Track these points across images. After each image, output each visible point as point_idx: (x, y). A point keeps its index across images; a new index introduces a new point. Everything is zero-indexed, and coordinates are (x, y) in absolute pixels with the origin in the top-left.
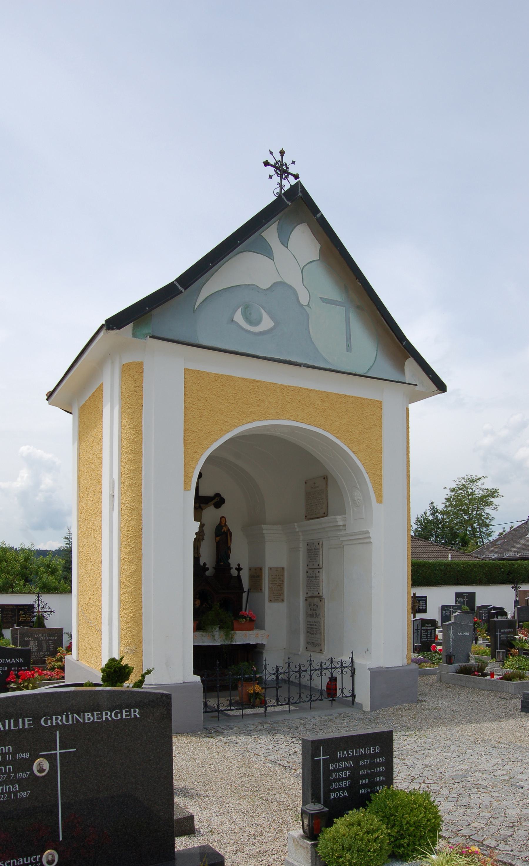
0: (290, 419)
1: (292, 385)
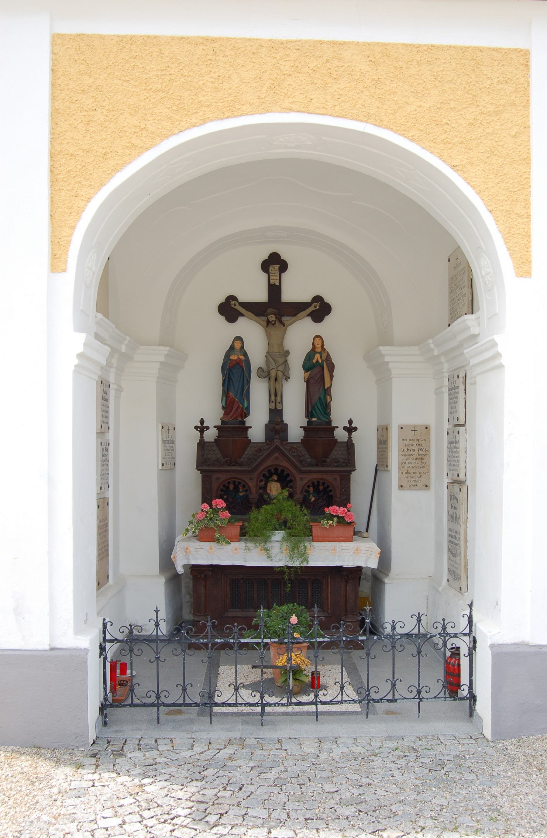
0: (291, 110)
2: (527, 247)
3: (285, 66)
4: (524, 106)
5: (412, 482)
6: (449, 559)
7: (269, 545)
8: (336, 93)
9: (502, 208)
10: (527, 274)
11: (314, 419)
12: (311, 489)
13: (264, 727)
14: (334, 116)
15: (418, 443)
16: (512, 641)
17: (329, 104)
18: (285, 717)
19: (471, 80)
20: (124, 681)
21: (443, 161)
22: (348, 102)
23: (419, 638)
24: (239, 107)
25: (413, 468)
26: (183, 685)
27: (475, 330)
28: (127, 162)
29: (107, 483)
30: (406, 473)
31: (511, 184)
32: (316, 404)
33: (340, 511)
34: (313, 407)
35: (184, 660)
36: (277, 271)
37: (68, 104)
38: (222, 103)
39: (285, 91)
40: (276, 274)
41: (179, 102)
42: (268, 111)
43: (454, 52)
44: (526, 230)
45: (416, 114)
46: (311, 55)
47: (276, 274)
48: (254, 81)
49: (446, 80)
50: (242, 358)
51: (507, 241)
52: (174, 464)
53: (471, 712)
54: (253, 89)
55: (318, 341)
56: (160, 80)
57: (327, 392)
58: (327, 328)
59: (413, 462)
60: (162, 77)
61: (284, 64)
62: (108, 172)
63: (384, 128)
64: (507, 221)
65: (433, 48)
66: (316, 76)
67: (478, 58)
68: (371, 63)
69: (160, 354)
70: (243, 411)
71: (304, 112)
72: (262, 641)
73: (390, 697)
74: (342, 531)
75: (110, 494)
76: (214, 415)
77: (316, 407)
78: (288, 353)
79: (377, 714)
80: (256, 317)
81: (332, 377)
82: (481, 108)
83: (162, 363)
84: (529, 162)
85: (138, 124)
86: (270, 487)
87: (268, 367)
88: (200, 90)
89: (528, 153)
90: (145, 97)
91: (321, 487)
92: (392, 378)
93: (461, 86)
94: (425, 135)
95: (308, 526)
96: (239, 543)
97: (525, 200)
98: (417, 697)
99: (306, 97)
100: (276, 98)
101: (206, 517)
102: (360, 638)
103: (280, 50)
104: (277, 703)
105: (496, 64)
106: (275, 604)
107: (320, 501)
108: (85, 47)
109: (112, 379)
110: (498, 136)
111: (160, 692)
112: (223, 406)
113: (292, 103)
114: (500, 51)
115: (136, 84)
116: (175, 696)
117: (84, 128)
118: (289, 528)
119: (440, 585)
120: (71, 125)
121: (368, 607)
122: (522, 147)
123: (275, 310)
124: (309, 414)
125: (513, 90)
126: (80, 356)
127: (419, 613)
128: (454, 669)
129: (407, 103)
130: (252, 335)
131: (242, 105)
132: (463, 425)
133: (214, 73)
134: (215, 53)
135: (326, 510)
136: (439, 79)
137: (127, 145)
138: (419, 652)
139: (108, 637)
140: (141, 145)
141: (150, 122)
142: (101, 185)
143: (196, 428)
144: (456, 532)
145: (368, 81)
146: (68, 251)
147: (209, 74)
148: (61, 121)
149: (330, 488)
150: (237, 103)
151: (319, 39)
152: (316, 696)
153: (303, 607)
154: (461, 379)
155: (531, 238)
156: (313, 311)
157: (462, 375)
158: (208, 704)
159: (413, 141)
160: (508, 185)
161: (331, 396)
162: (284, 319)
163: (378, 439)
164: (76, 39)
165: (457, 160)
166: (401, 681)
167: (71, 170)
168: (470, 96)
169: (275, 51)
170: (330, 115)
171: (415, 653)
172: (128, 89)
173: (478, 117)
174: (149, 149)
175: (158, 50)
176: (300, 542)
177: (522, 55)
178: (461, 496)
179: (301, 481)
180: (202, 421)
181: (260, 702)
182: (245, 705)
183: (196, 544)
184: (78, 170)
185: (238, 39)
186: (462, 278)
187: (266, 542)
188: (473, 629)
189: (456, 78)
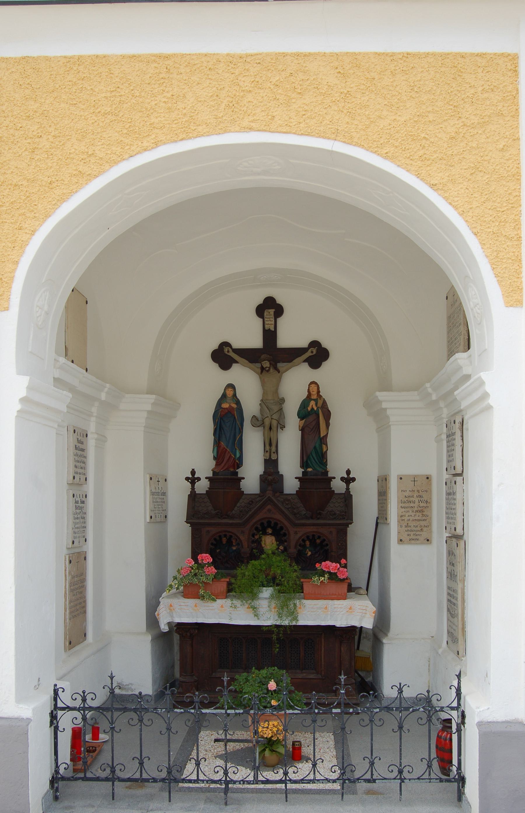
0: (251, 129)
1: (255, 52)
2: (518, 273)
3: (244, 81)
4: (512, 116)
5: (412, 535)
6: (448, 620)
7: (256, 603)
8: (301, 109)
9: (489, 230)
10: (519, 303)
11: (309, 470)
12: (308, 543)
13: (228, 807)
14: (298, 134)
15: (418, 494)
16: (503, 719)
17: (292, 120)
18: (254, 795)
19: (452, 90)
20: (93, 747)
21: (421, 179)
22: (314, 118)
23: (400, 712)
24: (195, 128)
25: (413, 520)
26: (139, 758)
27: (466, 370)
28: (74, 191)
29: (84, 537)
30: (406, 527)
31: (499, 203)
32: (311, 453)
33: (330, 566)
34: (308, 457)
35: (141, 730)
36: (272, 316)
37: (12, 131)
38: (176, 124)
39: (245, 109)
40: (271, 319)
41: (130, 125)
42: (225, 132)
43: (432, 60)
44: (516, 254)
45: (390, 129)
46: (273, 69)
47: (271, 319)
48: (211, 99)
49: (424, 91)
50: (234, 406)
51: (495, 267)
52: (166, 517)
53: (460, 795)
54: (210, 108)
55: (314, 388)
56: (110, 102)
57: (323, 441)
58: (323, 376)
59: (413, 514)
60: (112, 99)
61: (243, 79)
62: (54, 203)
63: (355, 145)
64: (495, 244)
65: (409, 56)
66: (279, 91)
67: (460, 65)
68: (339, 75)
69: (147, 402)
70: (235, 461)
71: (265, 131)
72: (226, 712)
73: (368, 776)
74: (334, 588)
75: (90, 548)
76: (205, 466)
77: (311, 457)
78: (283, 401)
79: (356, 794)
80: (250, 364)
81: (328, 425)
82: (463, 120)
83: (149, 412)
84: (518, 178)
85: (86, 150)
86: (265, 541)
87: (262, 415)
88: (152, 111)
89: (518, 168)
90: (93, 121)
91: (318, 541)
92: (390, 426)
93: (441, 97)
94: (401, 152)
95: (298, 582)
96: (225, 600)
97: (515, 221)
98: (399, 777)
99: (268, 115)
100: (235, 116)
101: (191, 572)
102: (334, 711)
103: (239, 64)
104: (242, 780)
105: (480, 70)
106: (254, 668)
107: (317, 555)
108: (30, 70)
109: (92, 428)
110: (483, 150)
111: (115, 765)
112: (214, 456)
113: (252, 121)
114: (484, 56)
115: (83, 107)
116: (131, 770)
117: (29, 157)
118: (278, 585)
119: (440, 647)
120: (15, 154)
121: (343, 676)
122: (511, 161)
123: (270, 357)
124: (304, 464)
125: (500, 99)
126: (23, 400)
127: (400, 684)
128: (445, 744)
129: (380, 117)
130: (246, 382)
131: (198, 126)
132: (460, 475)
133: (167, 92)
134: (168, 71)
135: (317, 565)
136: (416, 90)
137: (75, 172)
138: (401, 727)
139: (60, 704)
140: (89, 172)
141: (99, 148)
142: (46, 216)
143: (187, 479)
144: (454, 591)
145: (337, 95)
146: (11, 288)
147: (163, 93)
148: (4, 149)
149: (326, 542)
150: (192, 124)
151: (281, 51)
152: (286, 774)
153: (284, 671)
154: (458, 425)
155: (523, 262)
156: (310, 356)
157: (458, 420)
158: (167, 779)
159: (387, 159)
160: (496, 204)
161: (327, 445)
162: (279, 365)
163: (378, 491)
164: (21, 62)
165: (436, 178)
166: (380, 759)
167: (15, 201)
168: (451, 107)
169: (234, 66)
170: (295, 133)
171: (396, 729)
172: (75, 113)
173: (461, 130)
174: (97, 177)
175: (107, 70)
176: (290, 599)
177: (510, 60)
178: (459, 551)
179: (295, 535)
180: (193, 472)
181: (224, 779)
182: (207, 781)
183: (180, 601)
184: (22, 201)
185: (193, 55)
186: (458, 316)
187: (253, 600)
188: (462, 702)
189: (435, 88)
